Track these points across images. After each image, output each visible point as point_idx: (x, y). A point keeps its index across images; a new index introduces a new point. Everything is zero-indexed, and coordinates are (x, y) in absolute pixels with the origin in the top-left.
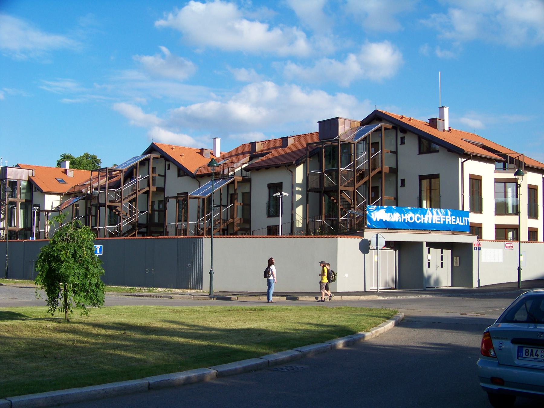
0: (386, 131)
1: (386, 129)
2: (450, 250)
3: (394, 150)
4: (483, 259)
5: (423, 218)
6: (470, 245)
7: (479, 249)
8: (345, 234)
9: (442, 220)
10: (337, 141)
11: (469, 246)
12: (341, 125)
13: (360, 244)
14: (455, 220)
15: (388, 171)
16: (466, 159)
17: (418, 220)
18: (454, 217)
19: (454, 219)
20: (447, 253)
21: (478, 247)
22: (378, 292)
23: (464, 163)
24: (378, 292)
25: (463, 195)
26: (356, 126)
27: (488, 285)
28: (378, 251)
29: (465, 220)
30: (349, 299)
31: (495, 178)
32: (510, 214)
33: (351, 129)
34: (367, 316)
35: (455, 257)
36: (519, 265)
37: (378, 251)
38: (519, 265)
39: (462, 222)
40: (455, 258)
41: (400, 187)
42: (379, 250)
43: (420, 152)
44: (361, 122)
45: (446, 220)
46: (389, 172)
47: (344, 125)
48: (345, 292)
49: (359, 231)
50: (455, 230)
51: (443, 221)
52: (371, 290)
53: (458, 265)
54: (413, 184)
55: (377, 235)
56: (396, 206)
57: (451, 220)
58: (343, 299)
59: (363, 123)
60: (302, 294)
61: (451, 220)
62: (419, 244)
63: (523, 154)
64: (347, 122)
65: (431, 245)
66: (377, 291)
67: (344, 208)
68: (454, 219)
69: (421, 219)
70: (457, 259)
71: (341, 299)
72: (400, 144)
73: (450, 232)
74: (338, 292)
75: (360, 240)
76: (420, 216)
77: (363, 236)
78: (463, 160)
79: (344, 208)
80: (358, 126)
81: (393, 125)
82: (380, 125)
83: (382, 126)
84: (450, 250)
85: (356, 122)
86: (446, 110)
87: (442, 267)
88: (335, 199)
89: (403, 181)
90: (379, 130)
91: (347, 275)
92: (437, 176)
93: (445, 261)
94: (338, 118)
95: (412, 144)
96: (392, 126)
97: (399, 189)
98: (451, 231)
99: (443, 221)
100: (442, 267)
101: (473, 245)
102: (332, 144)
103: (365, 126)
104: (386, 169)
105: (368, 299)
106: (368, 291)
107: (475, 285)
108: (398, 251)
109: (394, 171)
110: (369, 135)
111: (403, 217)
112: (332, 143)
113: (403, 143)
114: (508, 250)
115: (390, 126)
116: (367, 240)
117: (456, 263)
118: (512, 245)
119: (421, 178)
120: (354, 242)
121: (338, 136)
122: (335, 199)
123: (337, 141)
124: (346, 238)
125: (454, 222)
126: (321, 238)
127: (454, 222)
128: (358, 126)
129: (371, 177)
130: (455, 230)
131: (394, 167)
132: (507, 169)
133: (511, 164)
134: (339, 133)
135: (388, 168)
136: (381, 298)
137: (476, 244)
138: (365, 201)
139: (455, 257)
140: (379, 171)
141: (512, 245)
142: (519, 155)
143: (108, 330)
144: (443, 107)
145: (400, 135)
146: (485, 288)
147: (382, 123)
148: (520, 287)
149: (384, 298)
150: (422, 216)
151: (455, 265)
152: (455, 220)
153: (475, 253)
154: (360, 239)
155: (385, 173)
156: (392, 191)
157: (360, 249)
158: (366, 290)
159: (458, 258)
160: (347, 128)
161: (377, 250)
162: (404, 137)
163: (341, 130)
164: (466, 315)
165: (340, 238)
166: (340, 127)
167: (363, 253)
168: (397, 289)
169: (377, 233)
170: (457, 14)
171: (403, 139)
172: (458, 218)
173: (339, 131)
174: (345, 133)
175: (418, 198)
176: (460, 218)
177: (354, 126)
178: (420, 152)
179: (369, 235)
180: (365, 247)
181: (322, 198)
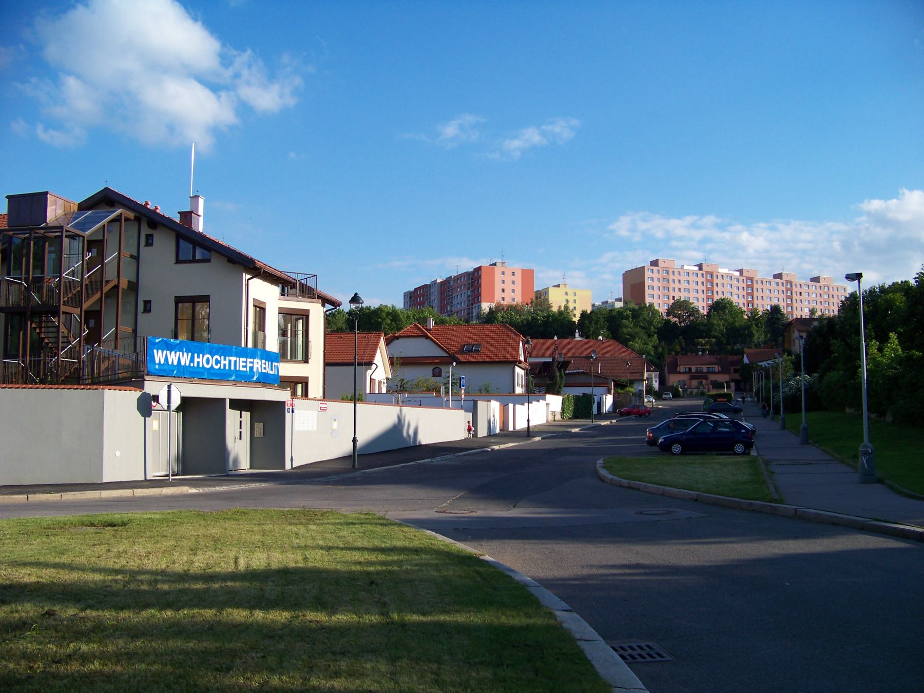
0: (127, 222)
1: (127, 219)
2: (249, 413)
3: (135, 254)
4: (297, 427)
5: (223, 362)
6: (282, 404)
7: (293, 411)
8: (106, 384)
9: (249, 365)
10: (60, 230)
11: (280, 405)
12: (51, 206)
13: (139, 400)
14: (244, 364)
15: (126, 286)
16: (251, 277)
17: (216, 364)
18: (245, 359)
19: (243, 362)
20: (246, 415)
21: (291, 408)
22: (171, 480)
23: (250, 281)
24: (171, 480)
25: (247, 329)
26: (72, 211)
27: (302, 466)
28: (170, 413)
29: (275, 366)
30: (145, 495)
31: (279, 307)
32: (299, 362)
33: (65, 215)
34: (340, 524)
35: (256, 424)
36: (355, 434)
37: (170, 413)
38: (355, 434)
39: (272, 370)
40: (256, 424)
41: (142, 313)
42: (172, 412)
43: (178, 261)
44: (79, 204)
45: (246, 364)
46: (128, 287)
47: (55, 207)
48: (115, 482)
49: (134, 379)
50: (265, 381)
51: (250, 367)
52: (154, 477)
53: (262, 436)
54: (164, 310)
55: (169, 387)
56: (175, 339)
57: (261, 366)
58: (136, 494)
59: (84, 206)
60: (35, 489)
61: (261, 366)
62: (218, 403)
63: (316, 276)
64: (60, 202)
65: (238, 404)
66: (169, 479)
67: (50, 343)
68: (243, 362)
69: (220, 363)
70: (259, 426)
71: (132, 494)
72: (145, 246)
73: (260, 385)
74: (104, 482)
75: (138, 394)
76: (219, 359)
77: (143, 388)
78: (248, 276)
79: (50, 343)
80: (74, 211)
81: (137, 215)
82: (119, 211)
83: (121, 214)
84: (249, 413)
85: (72, 204)
86: (201, 201)
87: (240, 439)
88: (37, 327)
89: (147, 303)
90: (117, 220)
91: (118, 453)
92: (205, 299)
93: (243, 430)
94: (46, 193)
95: (164, 245)
96: (135, 216)
97: (141, 317)
98: (260, 382)
99: (250, 367)
100: (240, 439)
101: (286, 405)
102: (45, 234)
103: (90, 212)
104: (124, 284)
105: (175, 494)
106: (150, 480)
107: (288, 466)
108: (181, 413)
109: (134, 287)
110: (104, 225)
111: (196, 360)
112: (44, 232)
113: (149, 243)
114: (323, 413)
115: (131, 215)
116: (149, 394)
117: (259, 432)
118: (326, 406)
119: (179, 300)
120: (131, 397)
121: (47, 223)
122: (37, 327)
123: (60, 230)
124: (128, 391)
125: (243, 367)
126: (15, 388)
127: (243, 367)
128: (74, 211)
129: (105, 294)
130: (265, 381)
131: (134, 280)
132: (286, 295)
133: (291, 288)
134: (47, 218)
135: (127, 282)
136: (194, 491)
137: (289, 403)
138: (86, 332)
139: (256, 424)
140: (113, 285)
141: (326, 406)
142: (309, 276)
143: (258, 610)
144: (197, 197)
145: (145, 230)
146: (299, 471)
147: (122, 210)
148: (356, 467)
149: (198, 491)
150: (223, 357)
151: (255, 436)
152: (244, 364)
153: (288, 416)
154: (138, 392)
155: (122, 288)
156: (130, 318)
157: (138, 409)
158: (147, 479)
159: (261, 424)
160: (60, 212)
161: (169, 412)
162: (152, 236)
163: (54, 213)
164: (447, 513)
165: (109, 389)
166: (49, 209)
167: (142, 416)
168: (179, 476)
169: (169, 384)
170: (72, 84)
171: (149, 238)
172: (267, 362)
173: (48, 214)
174: (57, 219)
175: (172, 331)
176: (270, 363)
177: (69, 211)
178: (178, 261)
179: (152, 386)
180: (146, 406)
181: (27, 322)
